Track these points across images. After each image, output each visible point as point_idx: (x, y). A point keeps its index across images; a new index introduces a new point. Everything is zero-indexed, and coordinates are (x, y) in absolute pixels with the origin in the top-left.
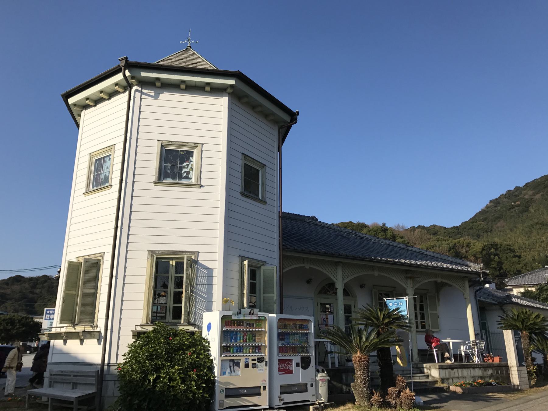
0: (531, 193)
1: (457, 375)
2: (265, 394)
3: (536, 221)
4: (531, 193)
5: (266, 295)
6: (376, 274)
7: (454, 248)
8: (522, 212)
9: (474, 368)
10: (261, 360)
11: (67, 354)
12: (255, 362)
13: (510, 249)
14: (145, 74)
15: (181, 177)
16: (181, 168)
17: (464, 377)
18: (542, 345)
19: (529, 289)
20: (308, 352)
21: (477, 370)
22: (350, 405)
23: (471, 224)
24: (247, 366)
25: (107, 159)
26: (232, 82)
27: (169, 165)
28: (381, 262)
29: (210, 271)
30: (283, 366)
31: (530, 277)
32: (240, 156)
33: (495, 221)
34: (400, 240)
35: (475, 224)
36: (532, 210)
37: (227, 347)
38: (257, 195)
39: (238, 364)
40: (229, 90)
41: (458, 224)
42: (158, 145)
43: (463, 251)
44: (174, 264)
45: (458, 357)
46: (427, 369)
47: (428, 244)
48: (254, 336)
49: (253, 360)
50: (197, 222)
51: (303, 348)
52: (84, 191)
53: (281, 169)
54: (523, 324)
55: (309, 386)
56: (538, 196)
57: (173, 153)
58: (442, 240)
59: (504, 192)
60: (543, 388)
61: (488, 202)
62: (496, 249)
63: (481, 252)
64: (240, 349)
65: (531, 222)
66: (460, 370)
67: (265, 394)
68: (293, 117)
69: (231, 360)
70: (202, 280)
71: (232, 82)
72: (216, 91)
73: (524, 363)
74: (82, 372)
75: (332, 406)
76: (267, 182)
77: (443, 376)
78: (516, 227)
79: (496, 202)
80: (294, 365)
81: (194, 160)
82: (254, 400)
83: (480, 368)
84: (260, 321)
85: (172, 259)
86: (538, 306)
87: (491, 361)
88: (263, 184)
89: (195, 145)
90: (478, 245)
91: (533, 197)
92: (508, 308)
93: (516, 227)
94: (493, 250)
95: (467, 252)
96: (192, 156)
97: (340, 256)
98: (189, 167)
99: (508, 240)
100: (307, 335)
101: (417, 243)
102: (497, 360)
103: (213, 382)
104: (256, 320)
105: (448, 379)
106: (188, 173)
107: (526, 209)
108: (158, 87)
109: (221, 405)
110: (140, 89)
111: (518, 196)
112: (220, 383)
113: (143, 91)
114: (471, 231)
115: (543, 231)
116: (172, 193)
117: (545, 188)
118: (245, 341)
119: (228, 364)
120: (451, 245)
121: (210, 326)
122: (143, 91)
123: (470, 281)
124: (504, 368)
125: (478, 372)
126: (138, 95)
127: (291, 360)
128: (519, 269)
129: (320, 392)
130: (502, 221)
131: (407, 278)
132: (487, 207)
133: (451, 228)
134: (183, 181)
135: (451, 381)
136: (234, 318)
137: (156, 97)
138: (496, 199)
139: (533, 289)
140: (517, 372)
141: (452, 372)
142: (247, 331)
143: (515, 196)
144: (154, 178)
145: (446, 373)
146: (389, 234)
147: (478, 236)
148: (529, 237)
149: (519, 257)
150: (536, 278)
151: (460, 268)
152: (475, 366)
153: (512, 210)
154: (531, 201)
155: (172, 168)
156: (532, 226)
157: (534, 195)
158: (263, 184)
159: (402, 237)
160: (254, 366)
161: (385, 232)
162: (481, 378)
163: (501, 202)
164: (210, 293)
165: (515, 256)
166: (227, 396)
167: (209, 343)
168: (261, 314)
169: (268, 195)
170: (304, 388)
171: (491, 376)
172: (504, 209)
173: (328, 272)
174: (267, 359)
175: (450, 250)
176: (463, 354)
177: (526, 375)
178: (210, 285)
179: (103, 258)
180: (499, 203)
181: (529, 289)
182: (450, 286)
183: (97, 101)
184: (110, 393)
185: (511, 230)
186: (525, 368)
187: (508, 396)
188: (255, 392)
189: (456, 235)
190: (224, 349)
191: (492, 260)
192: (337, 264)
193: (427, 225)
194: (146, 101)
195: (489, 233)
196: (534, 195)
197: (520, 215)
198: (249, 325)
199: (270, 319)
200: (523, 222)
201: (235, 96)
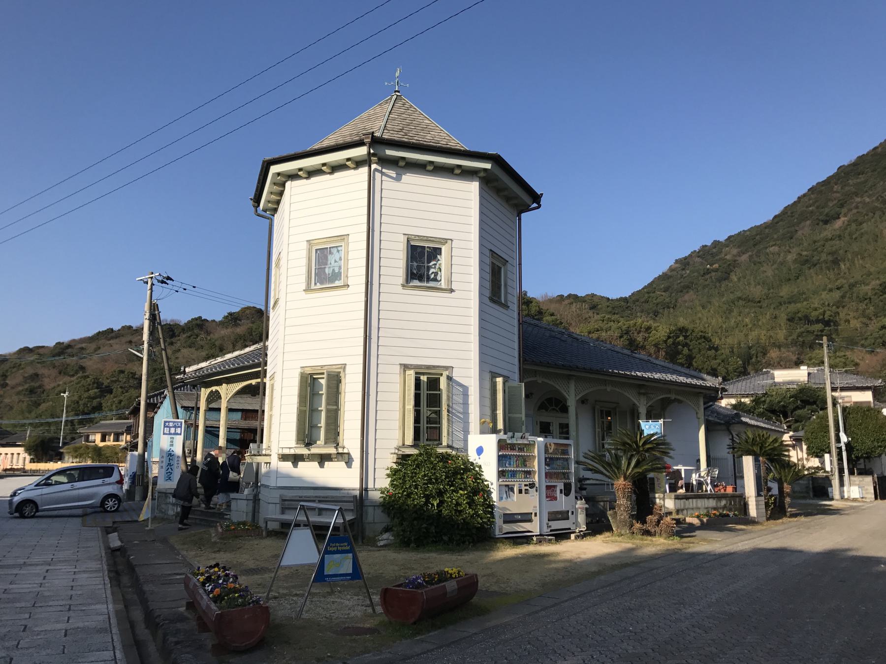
0: (735, 251)
1: (691, 506)
2: (536, 520)
3: (739, 294)
4: (735, 251)
5: (511, 415)
6: (609, 389)
7: (627, 333)
8: (720, 280)
9: (708, 498)
10: (532, 485)
11: (299, 479)
12: (527, 488)
13: (704, 337)
14: (390, 152)
15: (429, 279)
16: (429, 268)
17: (698, 508)
18: (780, 474)
19: (743, 400)
20: (569, 479)
21: (711, 500)
22: (607, 534)
23: (646, 295)
24: (520, 492)
25: (334, 251)
26: (488, 166)
27: (415, 264)
28: (613, 375)
29: (465, 390)
30: (549, 492)
31: (744, 383)
32: (488, 253)
33: (681, 291)
34: (549, 318)
35: (652, 295)
36: (734, 278)
37: (503, 471)
38: (500, 297)
39: (512, 490)
40: (482, 174)
41: (627, 294)
42: (403, 240)
43: (639, 339)
44: (426, 380)
45: (688, 486)
46: (660, 499)
47: (593, 325)
48: (525, 461)
49: (526, 485)
50: (450, 330)
51: (564, 474)
52: (304, 287)
53: (520, 264)
54: (761, 449)
55: (570, 514)
56: (744, 258)
57: (419, 250)
58: (609, 320)
59: (697, 248)
60: (780, 521)
61: (672, 262)
62: (686, 337)
63: (665, 342)
64: (514, 474)
65: (732, 296)
66: (694, 500)
67: (536, 520)
68: (536, 198)
69: (506, 486)
70: (458, 399)
71: (488, 166)
72: (467, 174)
73: (762, 493)
74: (332, 497)
75: (589, 534)
76: (509, 282)
77: (678, 507)
78: (710, 302)
79: (684, 263)
80: (558, 492)
81: (443, 259)
82: (526, 526)
83: (714, 498)
84: (531, 445)
85: (423, 374)
86: (753, 422)
87: (722, 491)
88: (506, 285)
89: (445, 241)
90: (661, 330)
91: (738, 258)
92: (735, 429)
93: (710, 302)
94: (681, 338)
95: (645, 339)
96: (440, 254)
97: (577, 368)
98: (437, 266)
99: (698, 321)
100: (567, 460)
101: (574, 324)
102: (730, 490)
103: (492, 507)
104: (526, 444)
105: (683, 510)
106: (436, 274)
107: (726, 277)
108: (401, 167)
109: (501, 529)
110: (380, 168)
111: (717, 255)
112: (499, 508)
113: (384, 170)
114: (646, 306)
115: (747, 310)
116: (420, 298)
117: (755, 245)
118: (517, 466)
119: (504, 489)
120: (624, 328)
121: (483, 451)
122: (384, 170)
123: (705, 397)
124: (737, 499)
125: (712, 503)
126: (378, 175)
127: (555, 486)
128: (715, 366)
129: (579, 520)
130: (692, 292)
131: (640, 394)
132: (671, 269)
133: (617, 300)
134: (431, 284)
135: (685, 512)
136: (508, 442)
137: (398, 179)
138: (686, 258)
139: (747, 401)
140: (754, 503)
141: (687, 502)
142: (519, 456)
143: (713, 255)
144: (401, 279)
145: (681, 503)
146: (534, 309)
147: (656, 313)
148: (727, 318)
149: (716, 349)
150: (752, 386)
151: (669, 375)
152: (708, 497)
153: (707, 276)
154: (733, 265)
155: (419, 267)
156: (733, 302)
157: (739, 254)
158: (506, 285)
159: (552, 315)
160: (527, 492)
161: (528, 306)
162: (715, 509)
163: (691, 263)
164: (466, 413)
165: (710, 349)
166: (505, 522)
167: (480, 467)
168: (531, 438)
169: (510, 297)
170: (565, 515)
171: (724, 507)
172: (696, 274)
173: (559, 386)
174: (537, 485)
175: (621, 337)
176: (694, 483)
177: (764, 506)
178: (466, 404)
179: (344, 371)
180: (688, 264)
181: (743, 400)
182: (680, 402)
183: (312, 173)
184: (370, 518)
185: (703, 307)
186: (763, 498)
187: (750, 527)
188: (526, 518)
189: (624, 311)
190: (501, 474)
191: (679, 353)
192: (569, 377)
193: (581, 293)
194: (388, 184)
195: (672, 310)
196: (740, 256)
197: (718, 284)
198: (521, 450)
199: (539, 442)
200: (721, 295)
201: (487, 181)
